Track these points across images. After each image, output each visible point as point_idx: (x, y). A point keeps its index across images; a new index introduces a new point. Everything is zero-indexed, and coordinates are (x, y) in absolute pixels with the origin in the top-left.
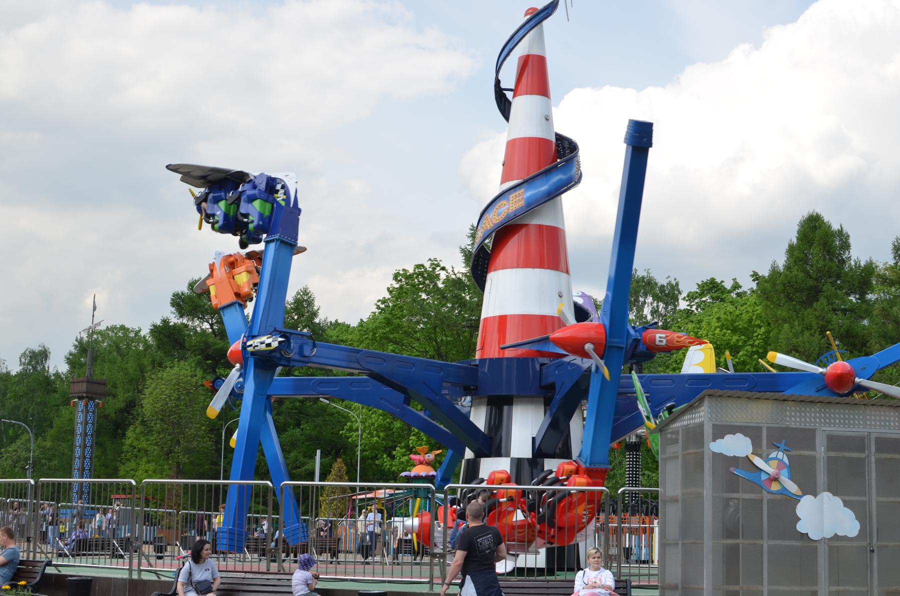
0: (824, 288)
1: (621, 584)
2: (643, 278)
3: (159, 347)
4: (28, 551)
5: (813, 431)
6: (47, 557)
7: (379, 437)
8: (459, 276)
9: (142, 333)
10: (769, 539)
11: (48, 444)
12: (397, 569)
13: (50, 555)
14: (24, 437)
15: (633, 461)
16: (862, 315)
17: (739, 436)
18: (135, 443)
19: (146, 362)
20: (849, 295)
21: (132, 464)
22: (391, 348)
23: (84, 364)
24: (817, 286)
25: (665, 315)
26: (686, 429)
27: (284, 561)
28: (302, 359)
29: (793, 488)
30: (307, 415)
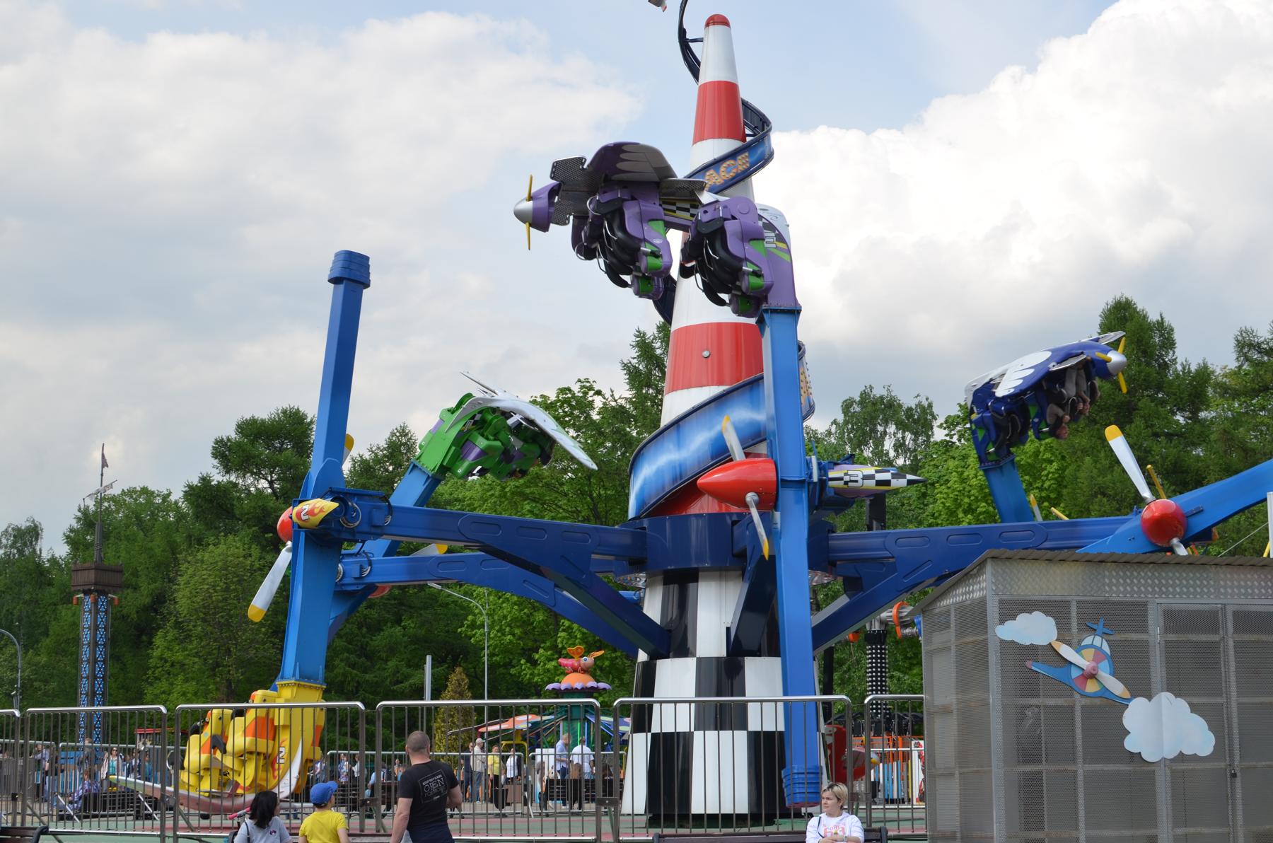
0: (1140, 404)
1: (873, 835)
2: (882, 398)
3: (197, 516)
4: (15, 813)
5: (1143, 606)
6: (41, 821)
7: (514, 635)
8: (622, 402)
9: (173, 498)
10: (1085, 762)
11: (43, 659)
12: (549, 822)
13: (45, 819)
14: (9, 651)
15: (876, 658)
16: (1195, 440)
17: (1037, 615)
18: (167, 655)
19: (179, 538)
20: (1175, 414)
21: (164, 685)
22: (528, 507)
23: (92, 544)
24: (1130, 402)
25: (915, 450)
26: (961, 608)
27: (384, 816)
28: (373, 530)
29: (1117, 688)
30: (411, 607)
